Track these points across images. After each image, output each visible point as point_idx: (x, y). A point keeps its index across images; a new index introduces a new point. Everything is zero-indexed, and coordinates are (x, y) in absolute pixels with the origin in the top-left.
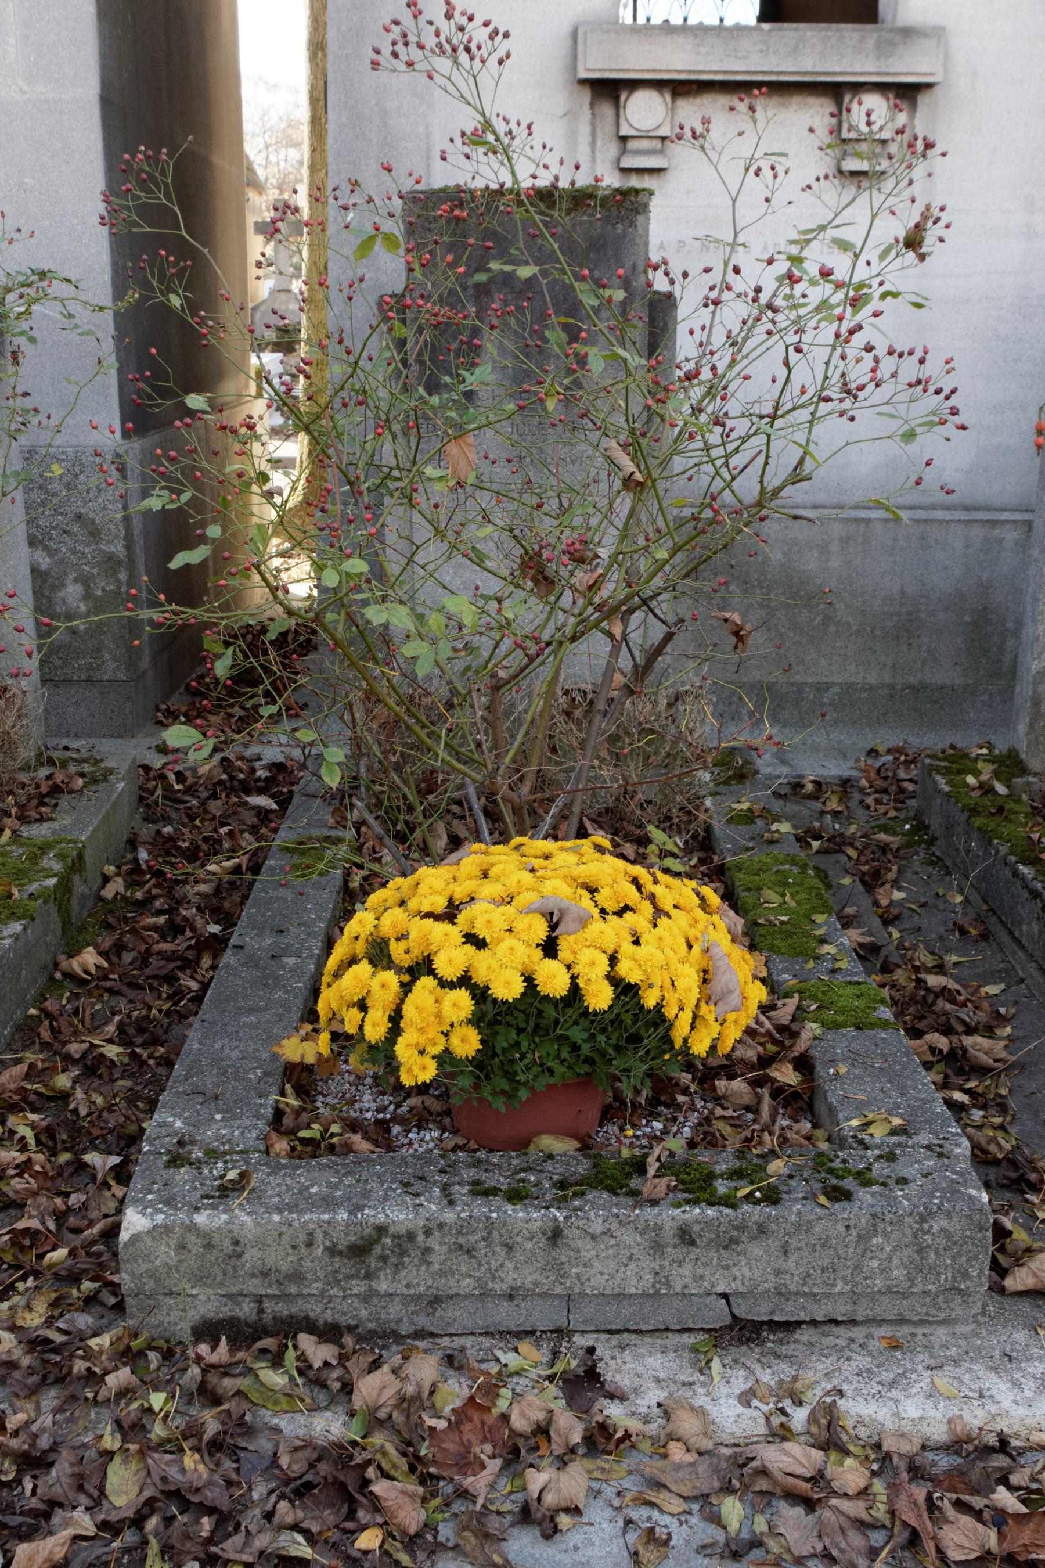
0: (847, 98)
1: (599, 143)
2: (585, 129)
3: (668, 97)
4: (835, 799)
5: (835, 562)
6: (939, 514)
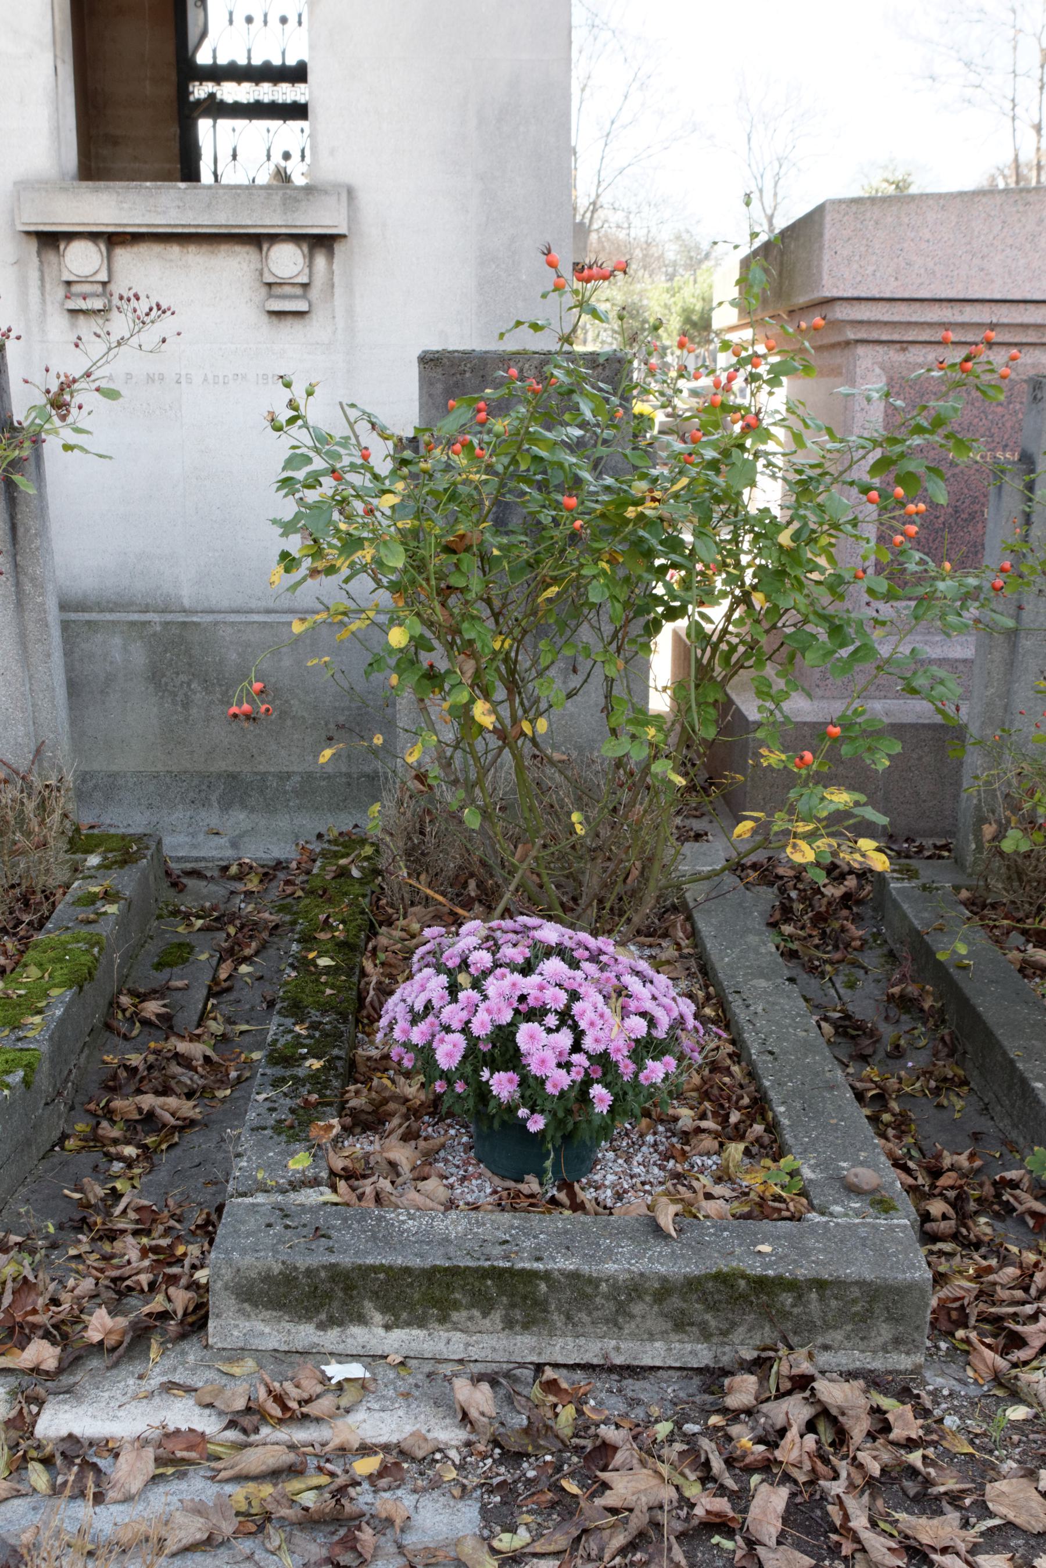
0: (265, 247)
1: (48, 286)
2: (34, 275)
3: (305, 249)
4: (256, 881)
5: (287, 662)
6: (256, 618)
